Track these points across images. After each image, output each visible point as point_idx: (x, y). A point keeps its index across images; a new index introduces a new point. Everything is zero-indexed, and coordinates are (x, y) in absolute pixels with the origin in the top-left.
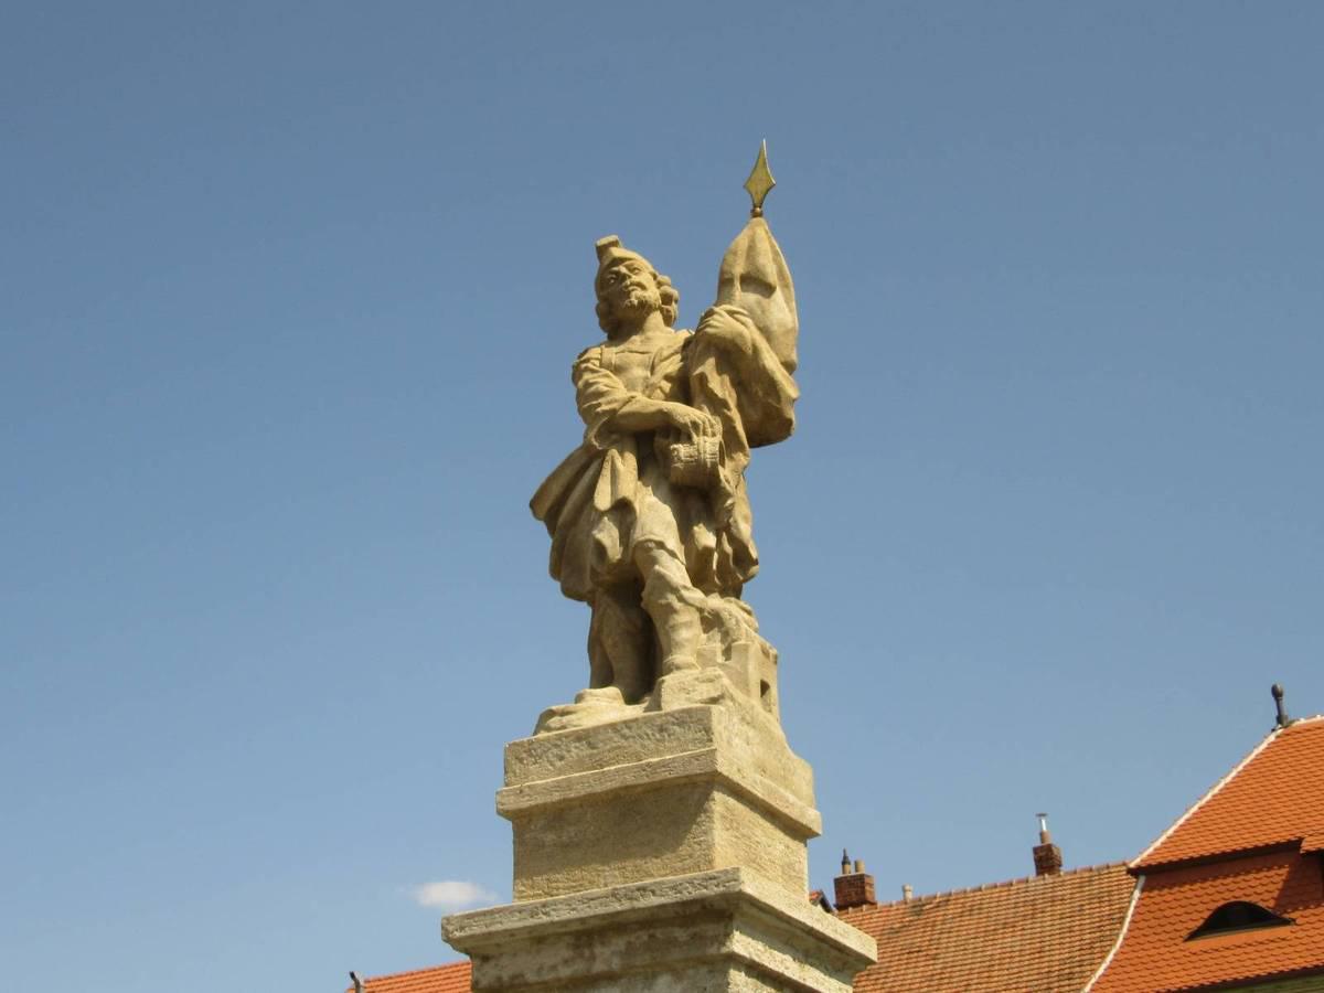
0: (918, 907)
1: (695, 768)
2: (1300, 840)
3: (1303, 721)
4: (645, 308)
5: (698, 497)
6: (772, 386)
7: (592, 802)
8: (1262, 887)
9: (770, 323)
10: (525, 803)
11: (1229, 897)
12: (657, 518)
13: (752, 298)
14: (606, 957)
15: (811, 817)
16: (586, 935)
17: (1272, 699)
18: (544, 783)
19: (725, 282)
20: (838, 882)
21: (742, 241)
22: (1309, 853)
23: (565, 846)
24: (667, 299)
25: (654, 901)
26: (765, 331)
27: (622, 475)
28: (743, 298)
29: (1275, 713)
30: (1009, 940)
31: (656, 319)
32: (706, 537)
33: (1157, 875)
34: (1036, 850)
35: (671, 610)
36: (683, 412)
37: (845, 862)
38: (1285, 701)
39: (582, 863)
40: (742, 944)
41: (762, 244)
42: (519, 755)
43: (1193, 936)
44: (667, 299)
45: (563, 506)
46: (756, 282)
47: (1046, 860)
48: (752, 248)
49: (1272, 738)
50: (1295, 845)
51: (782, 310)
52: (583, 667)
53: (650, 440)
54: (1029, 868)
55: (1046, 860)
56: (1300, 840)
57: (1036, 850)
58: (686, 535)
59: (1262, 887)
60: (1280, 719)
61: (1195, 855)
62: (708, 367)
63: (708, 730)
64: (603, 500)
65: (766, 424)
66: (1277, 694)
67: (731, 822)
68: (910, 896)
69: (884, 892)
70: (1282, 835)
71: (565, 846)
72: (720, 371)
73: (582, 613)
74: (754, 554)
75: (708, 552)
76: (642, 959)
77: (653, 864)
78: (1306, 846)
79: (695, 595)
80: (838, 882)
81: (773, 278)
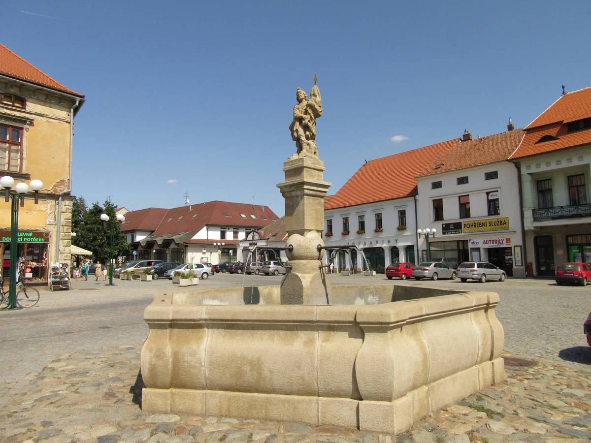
0: (481, 140)
1: (302, 166)
2: (563, 121)
3: (569, 93)
4: (302, 99)
5: (306, 128)
6: (317, 110)
7: (292, 169)
8: (553, 132)
9: (317, 101)
10: (286, 170)
11: (545, 134)
12: (301, 131)
13: (314, 97)
14: (293, 189)
15: (323, 168)
16: (291, 186)
17: (562, 89)
18: (288, 167)
19: (311, 95)
20: (464, 136)
21: (313, 89)
22: (565, 124)
23: (290, 175)
24: (305, 97)
25: (296, 182)
26: (315, 102)
27: (297, 125)
28: (313, 97)
29: (562, 91)
30: (499, 146)
31: (304, 100)
32: (308, 133)
33: (529, 131)
34: (508, 126)
35: (303, 144)
36: (304, 116)
37: (465, 131)
38: (565, 89)
39: (292, 177)
40: (305, 187)
41: (316, 89)
42: (285, 164)
43: (536, 143)
44: (305, 97)
45: (291, 128)
46: (315, 95)
47: (510, 128)
48: (314, 90)
49: (561, 98)
50: (561, 122)
51: (318, 99)
52: (296, 152)
53: (300, 120)
54: (506, 130)
55: (510, 128)
56: (563, 121)
57: (508, 126)
58: (305, 133)
59: (553, 132)
60: (563, 93)
61: (541, 125)
62: (308, 109)
63: (303, 161)
64: (295, 129)
65: (317, 115)
66: (563, 87)
67: (308, 171)
68: (479, 137)
69: (474, 137)
70: (559, 120)
71: (290, 175)
72: (310, 108)
73: (295, 142)
74: (315, 134)
75: (308, 135)
76: (296, 189)
77: (298, 177)
78: (564, 122)
79: (306, 141)
80: (464, 136)
81: (317, 94)
